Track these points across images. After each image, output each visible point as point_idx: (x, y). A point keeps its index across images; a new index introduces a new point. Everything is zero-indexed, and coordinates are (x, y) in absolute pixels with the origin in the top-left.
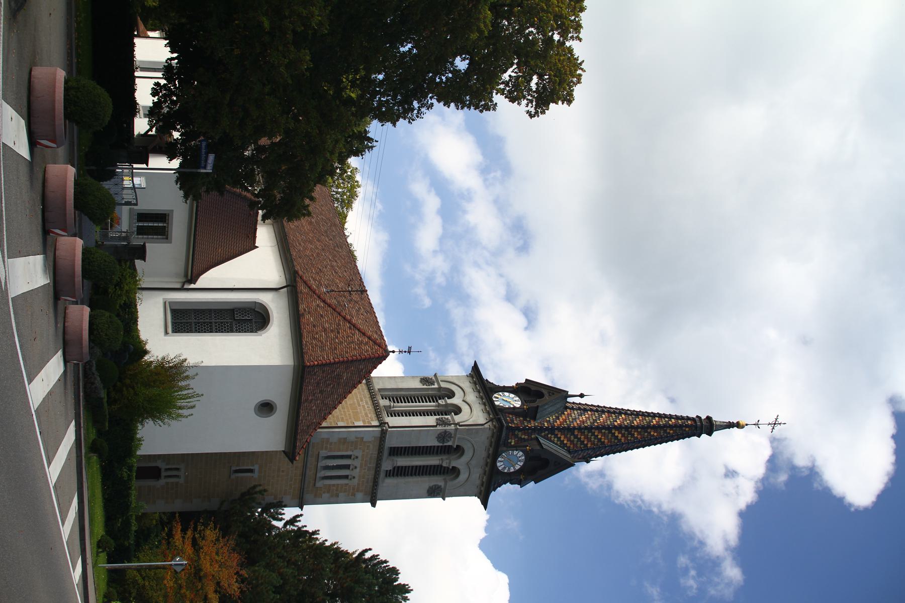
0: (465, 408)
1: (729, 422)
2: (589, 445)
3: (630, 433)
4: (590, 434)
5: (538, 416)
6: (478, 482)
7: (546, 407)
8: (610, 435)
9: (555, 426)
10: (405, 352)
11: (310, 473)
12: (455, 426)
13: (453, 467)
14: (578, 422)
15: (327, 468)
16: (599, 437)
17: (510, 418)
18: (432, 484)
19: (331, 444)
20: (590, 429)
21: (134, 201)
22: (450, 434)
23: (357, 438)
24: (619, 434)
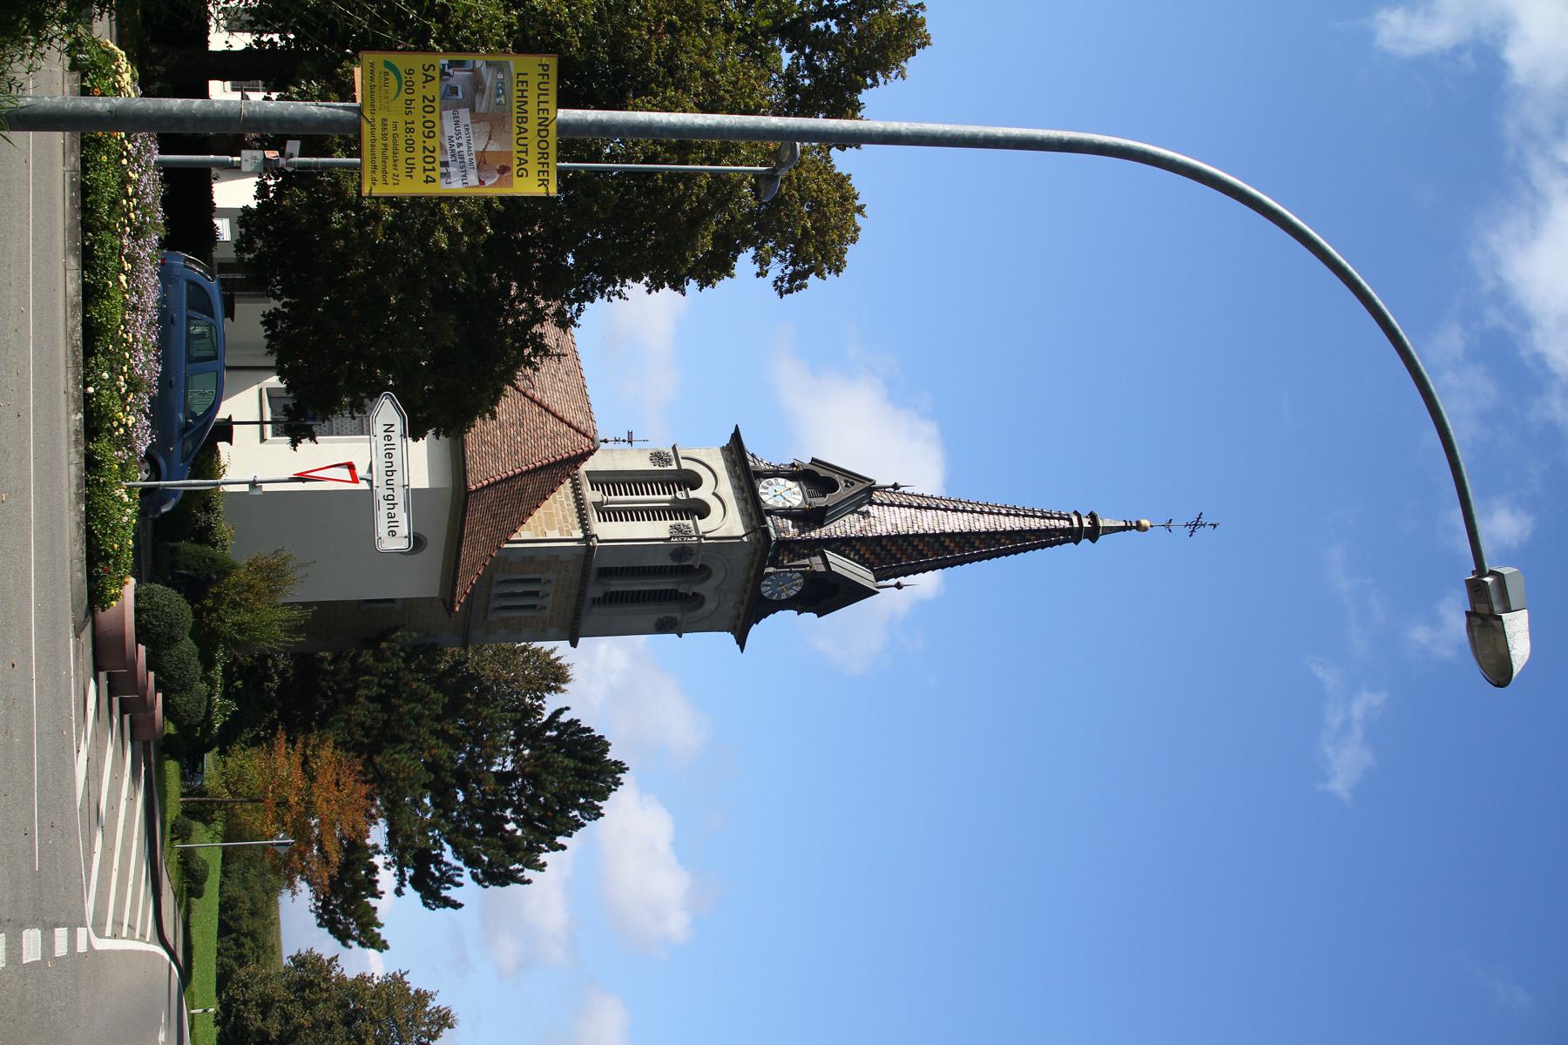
4: (906, 544)
10: (624, 441)
16: (920, 547)
21: (212, 353)
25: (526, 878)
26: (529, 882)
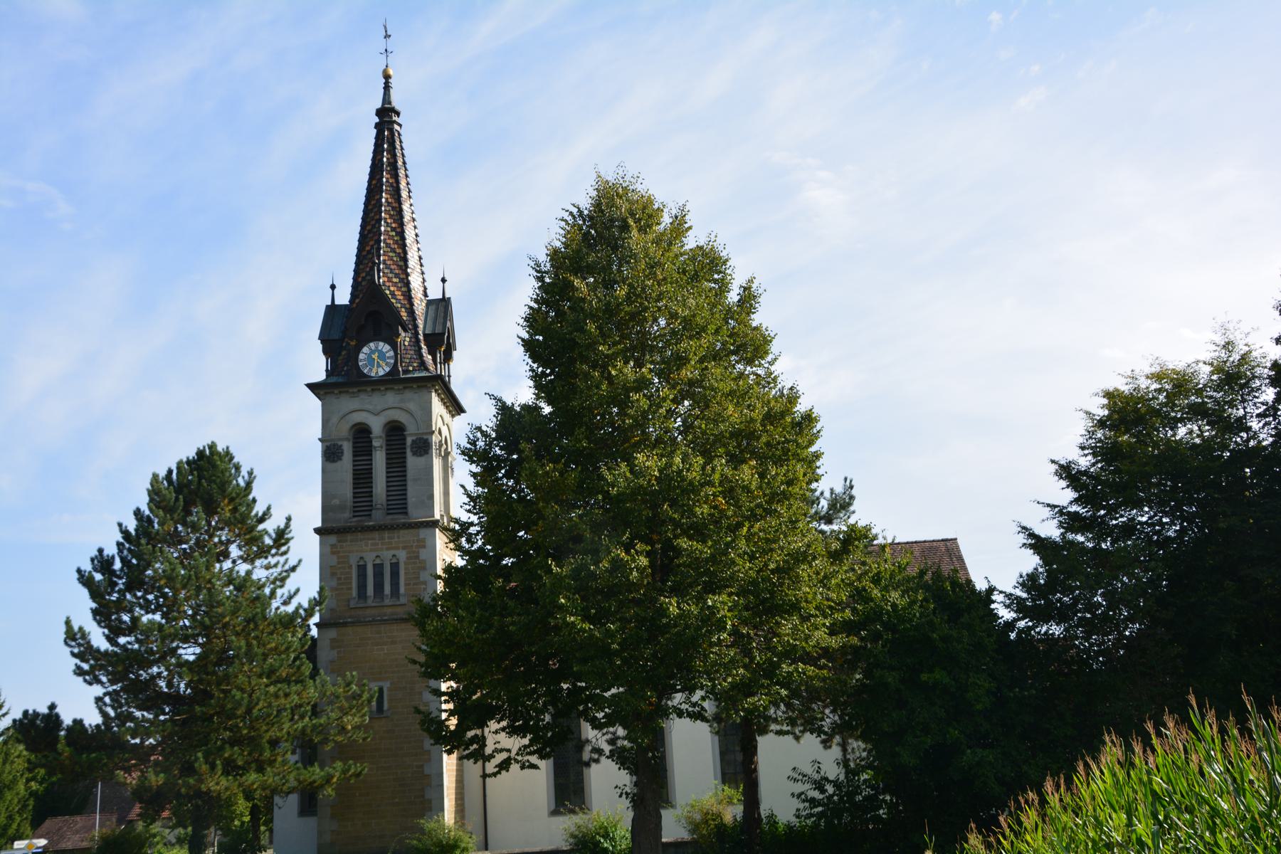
15: (379, 586)
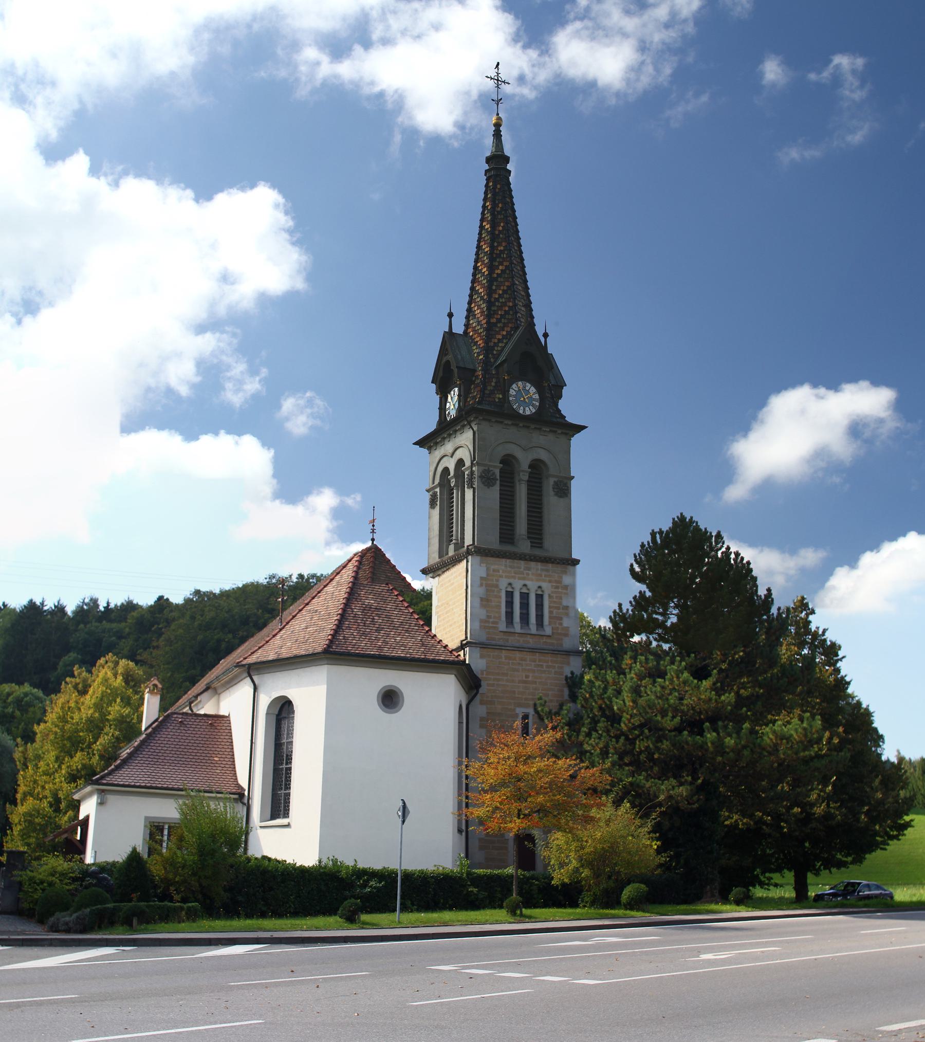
0: (460, 454)
1: (493, 135)
2: (511, 304)
3: (499, 256)
4: (497, 304)
5: (471, 367)
6: (551, 437)
7: (459, 357)
8: (499, 279)
9: (484, 346)
10: (373, 526)
11: (531, 642)
12: (475, 466)
13: (530, 467)
14: (482, 318)
15: (525, 618)
16: (501, 292)
17: (470, 401)
18: (552, 493)
19: (489, 617)
20: (490, 304)
22: (484, 471)
23: (481, 585)
24: (498, 269)
25: (766, 592)
26: (769, 590)
